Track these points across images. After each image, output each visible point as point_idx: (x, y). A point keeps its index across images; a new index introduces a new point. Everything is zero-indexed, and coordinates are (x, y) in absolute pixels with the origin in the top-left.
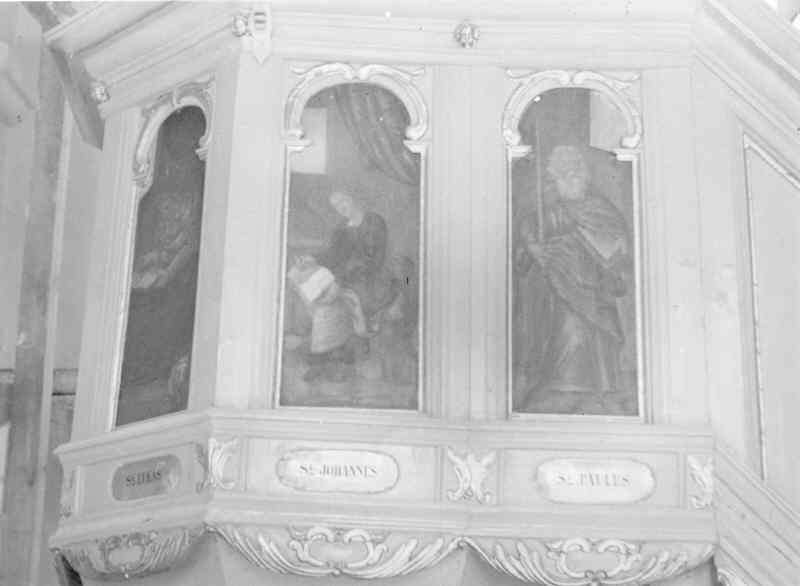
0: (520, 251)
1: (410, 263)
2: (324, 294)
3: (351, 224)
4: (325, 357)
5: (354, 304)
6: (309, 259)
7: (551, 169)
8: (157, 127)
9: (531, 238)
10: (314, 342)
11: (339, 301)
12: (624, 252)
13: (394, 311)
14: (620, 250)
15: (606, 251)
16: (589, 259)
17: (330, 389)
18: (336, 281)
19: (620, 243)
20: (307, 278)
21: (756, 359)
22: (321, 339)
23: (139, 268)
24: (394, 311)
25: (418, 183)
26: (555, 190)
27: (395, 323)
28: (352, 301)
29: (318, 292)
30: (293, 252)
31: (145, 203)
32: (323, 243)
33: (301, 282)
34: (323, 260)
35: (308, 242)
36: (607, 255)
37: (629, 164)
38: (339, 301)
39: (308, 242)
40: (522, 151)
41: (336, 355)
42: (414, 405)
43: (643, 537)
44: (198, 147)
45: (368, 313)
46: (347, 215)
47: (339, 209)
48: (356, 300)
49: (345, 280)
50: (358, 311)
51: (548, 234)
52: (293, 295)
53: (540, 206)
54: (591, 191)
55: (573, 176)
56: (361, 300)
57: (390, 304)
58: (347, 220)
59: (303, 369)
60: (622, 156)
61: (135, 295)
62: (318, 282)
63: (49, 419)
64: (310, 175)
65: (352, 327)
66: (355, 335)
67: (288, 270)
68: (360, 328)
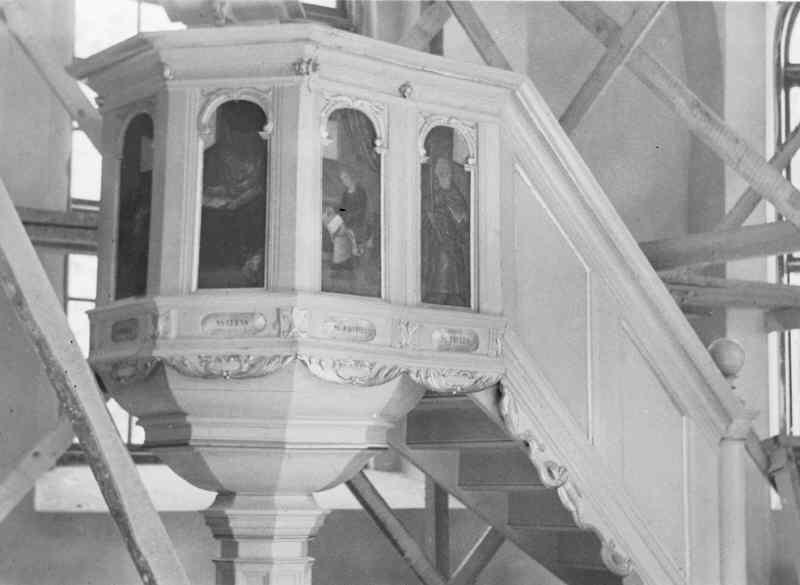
8: (219, 104)
13: (370, 243)
16: (452, 223)
17: (342, 283)
19: (464, 216)
20: (331, 219)
22: (339, 256)
23: (207, 192)
26: (438, 183)
30: (325, 204)
31: (208, 153)
32: (337, 200)
37: (469, 173)
38: (345, 235)
42: (379, 296)
43: (137, 574)
44: (262, 130)
49: (348, 223)
50: (354, 241)
51: (435, 207)
52: (325, 231)
54: (453, 184)
60: (467, 169)
61: (205, 211)
62: (336, 222)
63: (667, 292)
68: (355, 251)
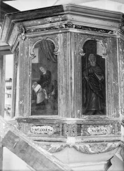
0: (83, 78)
1: (56, 81)
2: (39, 90)
3: (44, 74)
4: (39, 104)
5: (45, 92)
6: (36, 82)
7: (89, 59)
9: (85, 75)
10: (37, 101)
11: (42, 91)
12: (103, 78)
13: (53, 93)
14: (102, 79)
15: (100, 78)
17: (41, 111)
18: (41, 87)
21: (14, 44)
22: (39, 100)
24: (53, 93)
25: (82, 75)
27: (53, 96)
28: (44, 91)
29: (38, 90)
30: (33, 81)
33: (34, 88)
34: (39, 83)
35: (36, 79)
36: (100, 80)
38: (42, 91)
39: (36, 79)
40: (83, 54)
41: (42, 104)
45: (48, 94)
46: (43, 72)
47: (42, 70)
48: (45, 91)
49: (43, 87)
50: (46, 93)
53: (87, 67)
55: (94, 61)
56: (46, 91)
57: (52, 91)
58: (43, 73)
59: (36, 107)
62: (38, 88)
64: (36, 63)
65: (45, 97)
66: (45, 99)
67: (32, 86)
68: (46, 97)
